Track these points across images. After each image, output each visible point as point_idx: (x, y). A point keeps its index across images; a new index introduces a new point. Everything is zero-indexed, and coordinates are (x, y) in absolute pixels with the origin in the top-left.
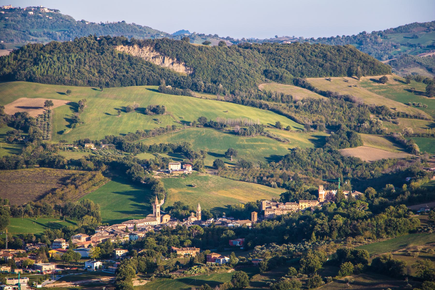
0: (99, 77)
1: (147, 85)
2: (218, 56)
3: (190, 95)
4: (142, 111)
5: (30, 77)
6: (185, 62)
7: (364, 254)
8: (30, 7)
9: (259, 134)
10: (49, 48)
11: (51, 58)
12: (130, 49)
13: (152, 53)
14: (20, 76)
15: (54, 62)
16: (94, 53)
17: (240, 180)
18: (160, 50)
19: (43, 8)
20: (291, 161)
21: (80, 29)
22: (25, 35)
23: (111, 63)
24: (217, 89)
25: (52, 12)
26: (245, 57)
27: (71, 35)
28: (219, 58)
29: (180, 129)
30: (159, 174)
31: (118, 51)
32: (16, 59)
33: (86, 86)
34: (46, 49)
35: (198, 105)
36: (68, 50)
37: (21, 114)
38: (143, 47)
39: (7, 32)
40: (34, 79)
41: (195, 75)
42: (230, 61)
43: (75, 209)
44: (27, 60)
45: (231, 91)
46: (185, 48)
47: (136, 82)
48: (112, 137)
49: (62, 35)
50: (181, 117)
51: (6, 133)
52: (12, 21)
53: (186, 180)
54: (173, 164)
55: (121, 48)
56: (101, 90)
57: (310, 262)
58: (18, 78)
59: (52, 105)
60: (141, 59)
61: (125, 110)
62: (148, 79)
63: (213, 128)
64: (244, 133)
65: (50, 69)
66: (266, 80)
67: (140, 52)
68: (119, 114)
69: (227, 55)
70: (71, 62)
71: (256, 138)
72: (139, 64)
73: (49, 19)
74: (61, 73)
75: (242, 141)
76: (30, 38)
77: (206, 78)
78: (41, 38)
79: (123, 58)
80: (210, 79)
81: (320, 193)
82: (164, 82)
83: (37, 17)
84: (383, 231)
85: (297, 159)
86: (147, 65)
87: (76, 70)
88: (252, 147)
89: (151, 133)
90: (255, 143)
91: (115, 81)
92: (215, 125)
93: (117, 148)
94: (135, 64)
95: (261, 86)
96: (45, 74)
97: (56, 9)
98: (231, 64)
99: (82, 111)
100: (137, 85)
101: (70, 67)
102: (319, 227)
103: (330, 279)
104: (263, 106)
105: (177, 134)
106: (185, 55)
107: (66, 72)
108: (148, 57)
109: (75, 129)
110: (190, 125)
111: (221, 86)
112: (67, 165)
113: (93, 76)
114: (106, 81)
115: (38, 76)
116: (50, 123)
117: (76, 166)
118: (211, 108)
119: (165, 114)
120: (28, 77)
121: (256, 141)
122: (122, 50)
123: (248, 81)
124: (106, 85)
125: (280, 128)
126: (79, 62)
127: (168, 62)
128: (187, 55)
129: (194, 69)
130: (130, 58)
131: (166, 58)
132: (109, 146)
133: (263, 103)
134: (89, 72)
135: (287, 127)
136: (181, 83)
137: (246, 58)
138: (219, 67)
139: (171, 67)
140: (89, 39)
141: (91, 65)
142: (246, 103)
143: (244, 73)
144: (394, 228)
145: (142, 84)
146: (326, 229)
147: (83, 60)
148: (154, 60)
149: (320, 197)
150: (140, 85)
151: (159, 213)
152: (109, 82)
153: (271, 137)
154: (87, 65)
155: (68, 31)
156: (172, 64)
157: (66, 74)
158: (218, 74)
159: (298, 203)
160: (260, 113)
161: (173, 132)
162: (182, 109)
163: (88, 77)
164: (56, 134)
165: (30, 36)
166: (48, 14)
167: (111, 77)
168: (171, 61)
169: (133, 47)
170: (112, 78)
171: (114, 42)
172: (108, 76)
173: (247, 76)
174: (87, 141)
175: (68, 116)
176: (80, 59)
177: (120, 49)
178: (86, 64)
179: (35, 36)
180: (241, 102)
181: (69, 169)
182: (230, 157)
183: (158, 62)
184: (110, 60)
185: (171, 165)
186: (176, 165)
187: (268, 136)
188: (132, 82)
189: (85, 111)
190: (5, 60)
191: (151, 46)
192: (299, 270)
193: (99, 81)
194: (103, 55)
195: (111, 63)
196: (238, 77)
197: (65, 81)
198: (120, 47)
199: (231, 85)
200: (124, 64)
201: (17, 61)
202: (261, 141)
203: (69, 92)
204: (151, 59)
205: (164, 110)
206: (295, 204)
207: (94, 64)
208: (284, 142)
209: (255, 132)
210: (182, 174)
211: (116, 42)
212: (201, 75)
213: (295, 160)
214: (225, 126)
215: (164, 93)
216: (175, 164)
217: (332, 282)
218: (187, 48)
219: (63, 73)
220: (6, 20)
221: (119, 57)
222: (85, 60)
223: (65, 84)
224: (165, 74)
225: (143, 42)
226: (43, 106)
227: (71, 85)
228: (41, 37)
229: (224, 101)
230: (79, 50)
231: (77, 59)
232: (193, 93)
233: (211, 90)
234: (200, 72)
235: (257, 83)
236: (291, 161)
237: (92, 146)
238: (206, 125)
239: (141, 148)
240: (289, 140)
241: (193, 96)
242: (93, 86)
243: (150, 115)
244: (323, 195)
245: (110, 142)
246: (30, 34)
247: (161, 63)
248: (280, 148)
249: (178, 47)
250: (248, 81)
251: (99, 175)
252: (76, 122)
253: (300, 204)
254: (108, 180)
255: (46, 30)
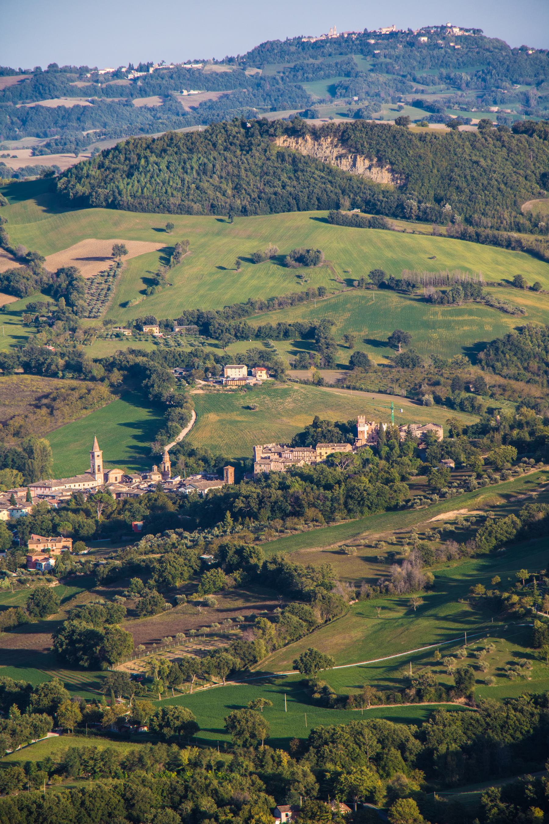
0: (234, 196)
1: (318, 209)
2: (455, 151)
3: (384, 227)
4: (280, 261)
5: (112, 201)
6: (392, 164)
7: (254, 553)
8: (429, 27)
9: (472, 300)
10: (158, 146)
11: (156, 164)
12: (300, 142)
13: (335, 150)
14: (96, 198)
15: (160, 170)
16: (235, 152)
17: (380, 392)
18: (350, 142)
19: (451, 27)
20: (503, 352)
21: (505, 66)
22: (404, 83)
23: (259, 170)
24: (441, 213)
25: (467, 34)
26: (510, 150)
27: (488, 77)
28: (456, 154)
29: (334, 293)
30: (205, 385)
31: (279, 146)
32: (103, 167)
33: (207, 214)
34: (154, 146)
35: (389, 246)
36: (191, 146)
37: (66, 271)
38: (320, 138)
39: (370, 80)
40: (119, 203)
41: (407, 188)
42: (474, 158)
43: (6, 456)
44: (118, 169)
45: (468, 216)
46: (394, 137)
47: (297, 204)
48: (196, 313)
49: (472, 79)
50: (346, 269)
51: (25, 308)
52: (385, 57)
53: (245, 396)
54: (231, 368)
55: (284, 142)
56: (230, 220)
57: (166, 569)
58: (93, 202)
59: (125, 253)
60: (315, 160)
61: (254, 260)
62: (318, 199)
63: (395, 290)
64: (442, 299)
65: (148, 185)
66: (540, 193)
67: (316, 147)
68: (238, 268)
69: (473, 147)
70: (189, 171)
71: (463, 307)
72: (309, 169)
73: (455, 49)
74: (166, 192)
75: (435, 314)
76: (412, 87)
77: (426, 192)
78: (434, 87)
79: (283, 160)
80: (432, 193)
81: (360, 429)
82: (346, 202)
83: (432, 47)
84: (342, 507)
85: (513, 348)
86: (322, 171)
87: (193, 186)
88: (447, 325)
89: (276, 302)
90: (456, 318)
91: (259, 203)
92: (397, 285)
93: (202, 332)
94: (302, 171)
95: (527, 206)
96: (139, 194)
97: (476, 28)
98: (475, 165)
99: (178, 262)
100: (299, 210)
101: (183, 180)
102: (243, 502)
103: (182, 599)
104: (513, 244)
105: (325, 303)
106: (392, 150)
107: (176, 188)
108: (328, 157)
109: (152, 297)
110: (353, 286)
111: (448, 206)
112: (62, 371)
113: (224, 195)
114: (243, 203)
115: (126, 198)
116: (113, 287)
117: (74, 372)
118: (412, 250)
119: (321, 264)
120: (110, 201)
121: (460, 313)
122: (286, 144)
123: (503, 195)
124: (241, 211)
125: (522, 287)
126: (203, 170)
127: (362, 164)
128: (395, 150)
129: (407, 178)
130: (295, 160)
131: (358, 157)
132: (188, 330)
133: (513, 239)
134: (218, 188)
135: (534, 285)
136: (377, 205)
137: (511, 151)
138: (452, 170)
139: (368, 173)
140: (231, 125)
141: (224, 175)
142: (482, 238)
143: (496, 180)
144: (359, 503)
145: (307, 209)
146: (253, 505)
147: (211, 165)
148: (339, 161)
149: (360, 436)
150: (304, 210)
151: (101, 467)
152: (248, 207)
153: (492, 306)
154: (215, 176)
155: (483, 72)
156: (370, 168)
157: (175, 193)
158: (449, 184)
159: (314, 448)
160: (500, 258)
161: (321, 298)
162: (355, 255)
163: (211, 197)
164: (117, 307)
165: (413, 84)
166: (458, 39)
167: (253, 196)
168: (367, 163)
169: (303, 138)
170: (254, 199)
171: (272, 130)
172: (249, 194)
173: (502, 186)
174: (150, 322)
175: (150, 272)
176: (205, 164)
177: (281, 142)
178: (214, 173)
179: (423, 84)
180: (475, 237)
181: (63, 377)
182: (398, 347)
183: (345, 165)
184: (260, 164)
185: (229, 370)
186: (237, 370)
187: (488, 304)
188: (289, 205)
189: (183, 263)
190: (82, 169)
191: (335, 136)
192: (147, 583)
193: (230, 205)
194: (248, 156)
195: (259, 170)
196: (485, 188)
197: (169, 207)
198: (282, 139)
199: (468, 205)
200: (282, 170)
201: (103, 170)
202: (471, 313)
203: (170, 227)
204: (334, 159)
205: (318, 257)
206: (310, 451)
207: (228, 173)
208: (513, 314)
209: (462, 295)
210: (243, 386)
211: (275, 130)
212: (417, 188)
213: (510, 350)
214: (414, 286)
215: (338, 224)
216: (235, 368)
217: (186, 604)
218: (398, 137)
219: (169, 191)
220: (374, 55)
221: (277, 158)
222: (214, 166)
223: (170, 212)
224: (353, 187)
225: (320, 129)
226: (110, 256)
227: (181, 213)
228: (434, 84)
229: (445, 236)
230: (211, 146)
231: (200, 164)
232: (389, 221)
233: (430, 217)
234: (416, 183)
235: (519, 200)
236: (503, 352)
237: (156, 331)
238: (383, 286)
239: (243, 331)
240: (525, 309)
241: (389, 229)
242: (219, 215)
243: (294, 267)
244: (366, 433)
245: (191, 321)
246: (415, 80)
247: (352, 168)
248: (497, 327)
249: (381, 137)
250: (503, 195)
251: (104, 389)
252: (157, 284)
253: (318, 451)
254: (116, 398)
255: (444, 71)
